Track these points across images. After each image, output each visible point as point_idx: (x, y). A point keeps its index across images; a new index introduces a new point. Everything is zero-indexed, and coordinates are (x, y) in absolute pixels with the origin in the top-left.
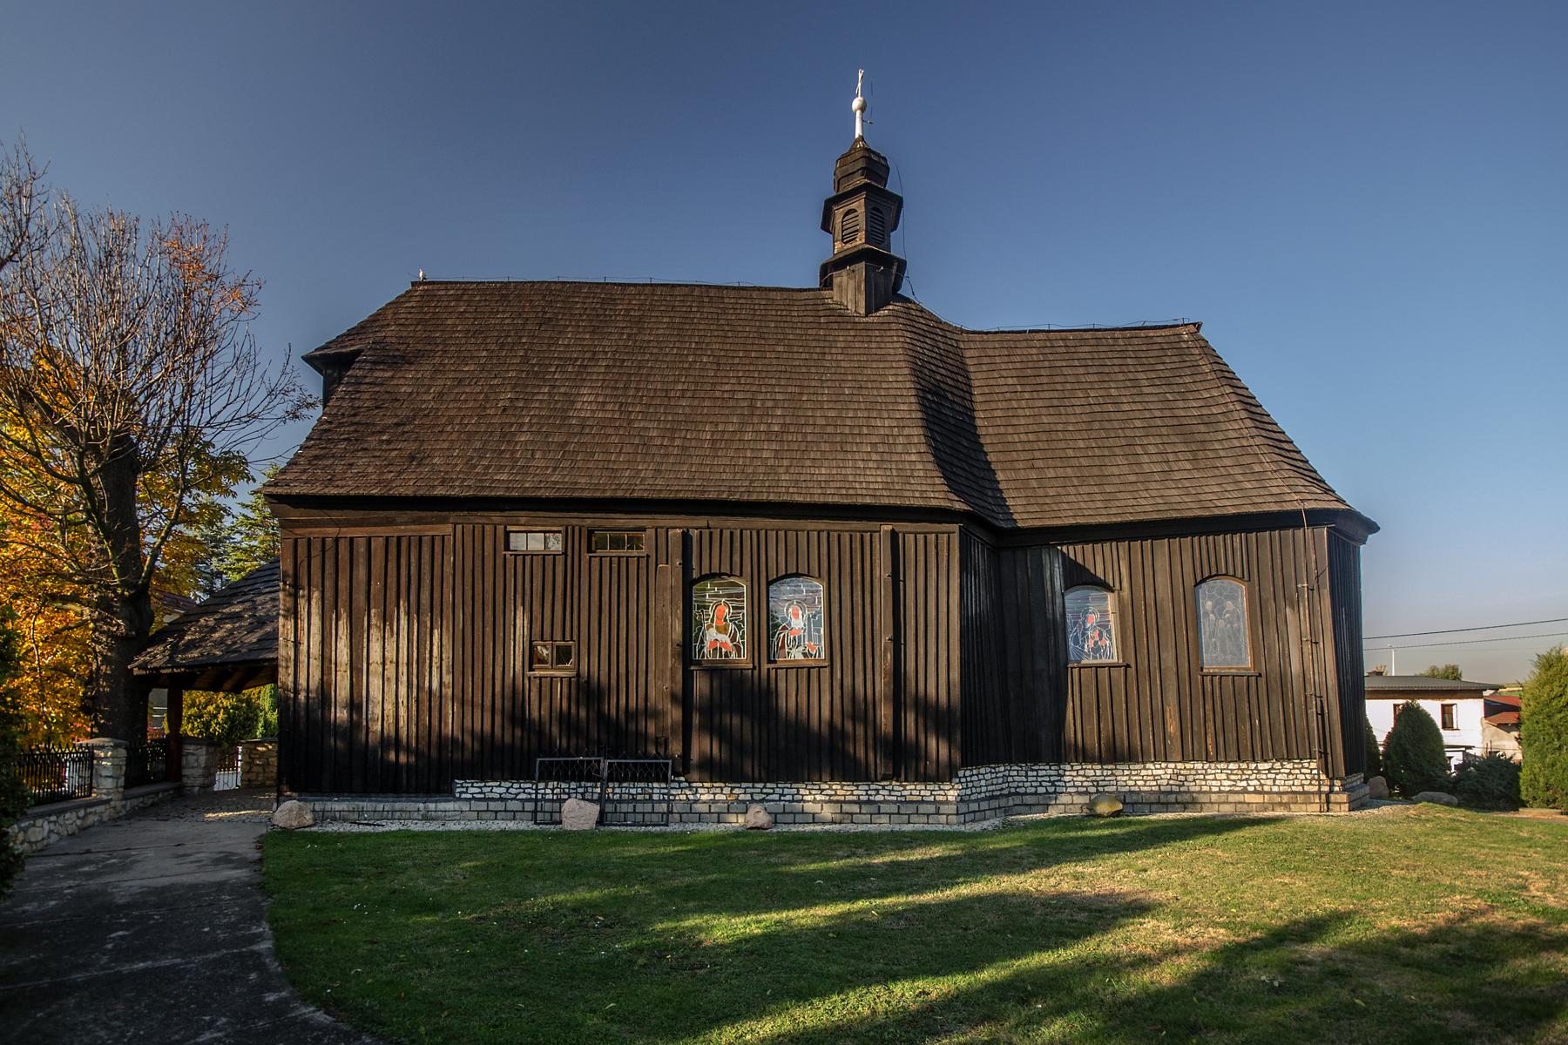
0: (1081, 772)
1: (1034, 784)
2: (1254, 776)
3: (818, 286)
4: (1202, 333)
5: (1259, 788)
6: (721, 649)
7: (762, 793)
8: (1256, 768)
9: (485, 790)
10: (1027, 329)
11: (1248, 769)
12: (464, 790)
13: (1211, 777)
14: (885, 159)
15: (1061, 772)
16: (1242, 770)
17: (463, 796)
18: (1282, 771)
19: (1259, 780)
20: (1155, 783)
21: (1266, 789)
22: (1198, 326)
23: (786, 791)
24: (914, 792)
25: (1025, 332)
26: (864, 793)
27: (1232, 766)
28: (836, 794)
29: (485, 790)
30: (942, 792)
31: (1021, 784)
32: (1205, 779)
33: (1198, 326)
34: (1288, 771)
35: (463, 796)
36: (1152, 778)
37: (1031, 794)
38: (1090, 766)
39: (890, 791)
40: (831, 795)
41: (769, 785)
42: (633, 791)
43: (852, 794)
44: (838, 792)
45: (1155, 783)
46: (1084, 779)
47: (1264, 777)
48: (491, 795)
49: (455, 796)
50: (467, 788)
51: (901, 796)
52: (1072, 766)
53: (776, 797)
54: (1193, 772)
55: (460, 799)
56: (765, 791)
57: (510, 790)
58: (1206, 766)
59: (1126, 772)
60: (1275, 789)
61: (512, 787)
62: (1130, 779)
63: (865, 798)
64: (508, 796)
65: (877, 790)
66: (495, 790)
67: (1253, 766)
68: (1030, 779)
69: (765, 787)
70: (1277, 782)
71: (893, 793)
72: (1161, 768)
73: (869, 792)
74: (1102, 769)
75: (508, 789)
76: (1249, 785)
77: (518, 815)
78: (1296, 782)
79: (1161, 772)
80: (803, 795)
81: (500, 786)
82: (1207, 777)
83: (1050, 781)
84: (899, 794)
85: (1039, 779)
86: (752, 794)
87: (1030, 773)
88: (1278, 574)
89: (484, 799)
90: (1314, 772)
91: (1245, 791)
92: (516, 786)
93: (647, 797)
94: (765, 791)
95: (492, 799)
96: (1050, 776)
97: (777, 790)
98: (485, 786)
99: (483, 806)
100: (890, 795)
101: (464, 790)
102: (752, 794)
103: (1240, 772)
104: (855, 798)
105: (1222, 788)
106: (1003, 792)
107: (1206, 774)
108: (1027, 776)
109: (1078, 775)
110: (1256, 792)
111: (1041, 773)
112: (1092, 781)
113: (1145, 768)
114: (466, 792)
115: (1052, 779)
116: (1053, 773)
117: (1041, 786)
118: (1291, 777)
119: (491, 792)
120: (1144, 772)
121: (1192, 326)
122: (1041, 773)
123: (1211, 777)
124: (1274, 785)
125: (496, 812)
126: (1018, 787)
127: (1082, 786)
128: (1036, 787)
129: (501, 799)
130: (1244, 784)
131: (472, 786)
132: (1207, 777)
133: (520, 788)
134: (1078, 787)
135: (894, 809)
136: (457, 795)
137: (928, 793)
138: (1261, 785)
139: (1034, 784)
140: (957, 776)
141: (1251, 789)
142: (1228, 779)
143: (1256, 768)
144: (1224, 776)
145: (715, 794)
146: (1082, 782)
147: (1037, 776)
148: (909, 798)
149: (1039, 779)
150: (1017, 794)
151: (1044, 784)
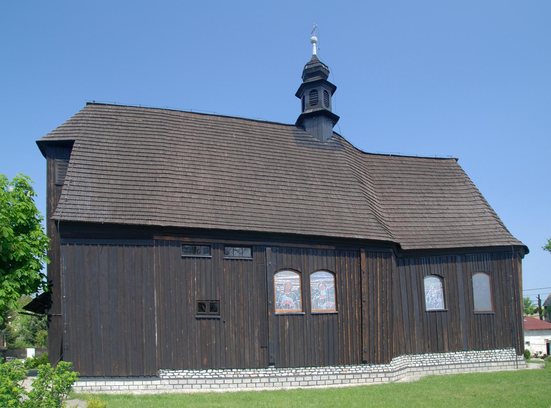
0: (432, 357)
1: (414, 363)
2: (493, 356)
3: (294, 124)
4: (458, 162)
5: (496, 360)
6: (289, 305)
7: (310, 372)
8: (495, 352)
9: (175, 374)
10: (390, 154)
11: (492, 352)
12: (164, 374)
13: (479, 356)
14: (327, 67)
15: (425, 357)
16: (490, 353)
17: (164, 377)
18: (503, 352)
19: (495, 357)
20: (459, 360)
21: (498, 360)
22: (457, 160)
23: (320, 370)
24: (375, 368)
25: (389, 155)
26: (354, 370)
27: (486, 351)
28: (342, 371)
29: (175, 374)
30: (386, 368)
31: (409, 363)
32: (477, 357)
33: (457, 160)
34: (505, 352)
35: (164, 377)
36: (458, 358)
37: (413, 367)
38: (435, 354)
39: (365, 368)
40: (340, 371)
41: (313, 368)
42: (250, 373)
43: (349, 370)
44: (344, 370)
45: (459, 360)
46: (434, 359)
47: (497, 355)
48: (179, 377)
49: (160, 378)
50: (166, 373)
51: (370, 370)
52: (429, 354)
53: (316, 373)
54: (473, 354)
55: (163, 379)
56: (311, 370)
57: (189, 374)
58: (477, 352)
59: (449, 356)
60: (501, 360)
61: (189, 372)
62: (451, 359)
63: (355, 372)
64: (188, 377)
65: (360, 368)
66: (180, 374)
67: (493, 351)
68: (413, 360)
69: (311, 369)
70: (502, 357)
71: (366, 369)
72: (462, 353)
73: (356, 369)
74: (440, 355)
75: (187, 373)
76: (492, 359)
77: (239, 385)
78: (508, 357)
79: (462, 355)
80: (328, 372)
81: (183, 372)
82: (478, 356)
83: (420, 361)
84: (369, 369)
85: (416, 360)
86: (305, 372)
87: (413, 358)
88: (174, 117)
89: (175, 379)
90: (514, 352)
91: (491, 362)
92: (191, 372)
93: (274, 375)
94: (311, 370)
95: (180, 379)
96: (420, 359)
97: (317, 370)
98: (175, 372)
99: (176, 382)
100: (365, 370)
101: (164, 374)
102: (305, 372)
103: (489, 354)
104: (351, 372)
105: (483, 361)
106: (408, 365)
107: (477, 355)
108: (411, 359)
109: (431, 358)
110: (495, 362)
111: (417, 358)
112: (436, 360)
113: (456, 354)
114: (166, 375)
115: (421, 360)
116: (422, 357)
117: (417, 363)
118: (506, 355)
119: (179, 375)
120: (455, 356)
121: (454, 160)
122: (417, 358)
123: (479, 356)
124: (501, 358)
125: (183, 385)
126: (408, 364)
127: (433, 363)
128: (415, 364)
129: (184, 378)
130: (490, 358)
131: (169, 372)
132: (478, 356)
133: (193, 373)
134: (431, 363)
135: (367, 376)
136: (161, 377)
137: (381, 368)
138: (497, 359)
139: (414, 363)
140: (392, 361)
141: (493, 360)
142: (485, 357)
143: (495, 352)
144: (484, 356)
145: (288, 373)
146: (432, 361)
147: (416, 359)
148: (373, 371)
149: (416, 360)
150: (408, 367)
151: (418, 362)
